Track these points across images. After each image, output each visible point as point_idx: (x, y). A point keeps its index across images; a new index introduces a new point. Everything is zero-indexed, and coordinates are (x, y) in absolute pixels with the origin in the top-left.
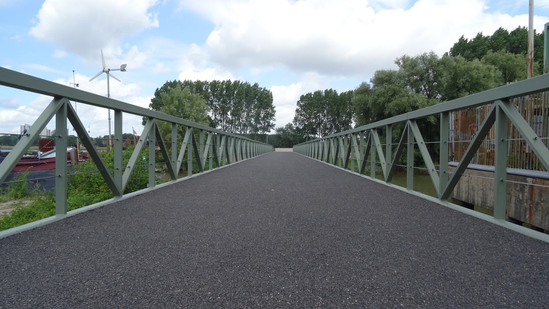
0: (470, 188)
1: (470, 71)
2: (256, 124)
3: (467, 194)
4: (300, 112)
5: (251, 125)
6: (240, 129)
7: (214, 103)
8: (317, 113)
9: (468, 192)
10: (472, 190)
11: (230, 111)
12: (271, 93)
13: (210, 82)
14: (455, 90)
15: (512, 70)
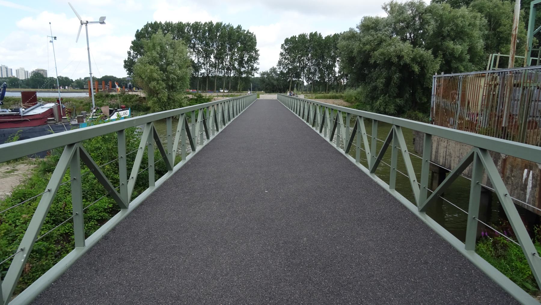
0: (447, 153)
1: (456, 18)
2: (240, 68)
3: (444, 159)
4: (284, 56)
5: (234, 68)
6: (223, 72)
7: (197, 46)
8: (302, 57)
9: (446, 157)
10: (449, 157)
11: (213, 55)
12: (255, 36)
13: (192, 24)
14: (440, 39)
15: (497, 18)
